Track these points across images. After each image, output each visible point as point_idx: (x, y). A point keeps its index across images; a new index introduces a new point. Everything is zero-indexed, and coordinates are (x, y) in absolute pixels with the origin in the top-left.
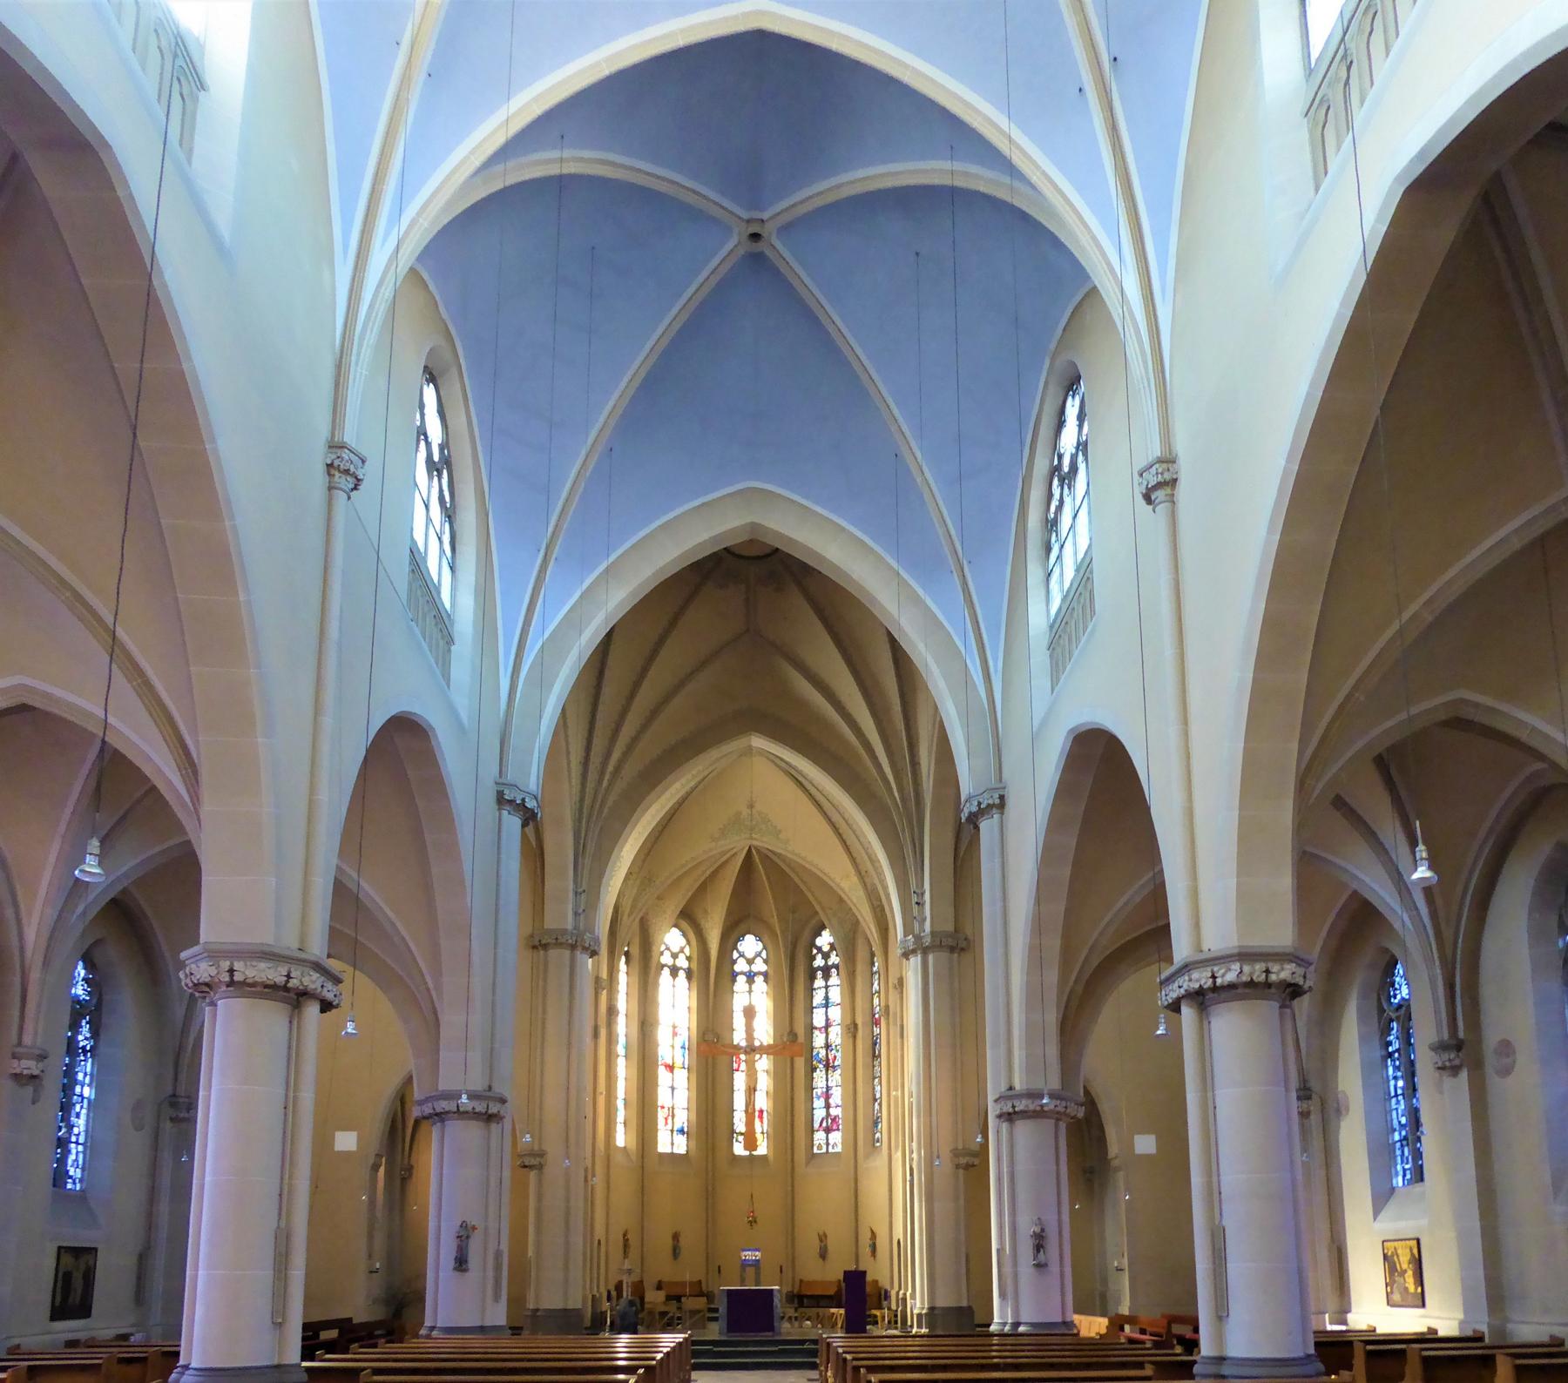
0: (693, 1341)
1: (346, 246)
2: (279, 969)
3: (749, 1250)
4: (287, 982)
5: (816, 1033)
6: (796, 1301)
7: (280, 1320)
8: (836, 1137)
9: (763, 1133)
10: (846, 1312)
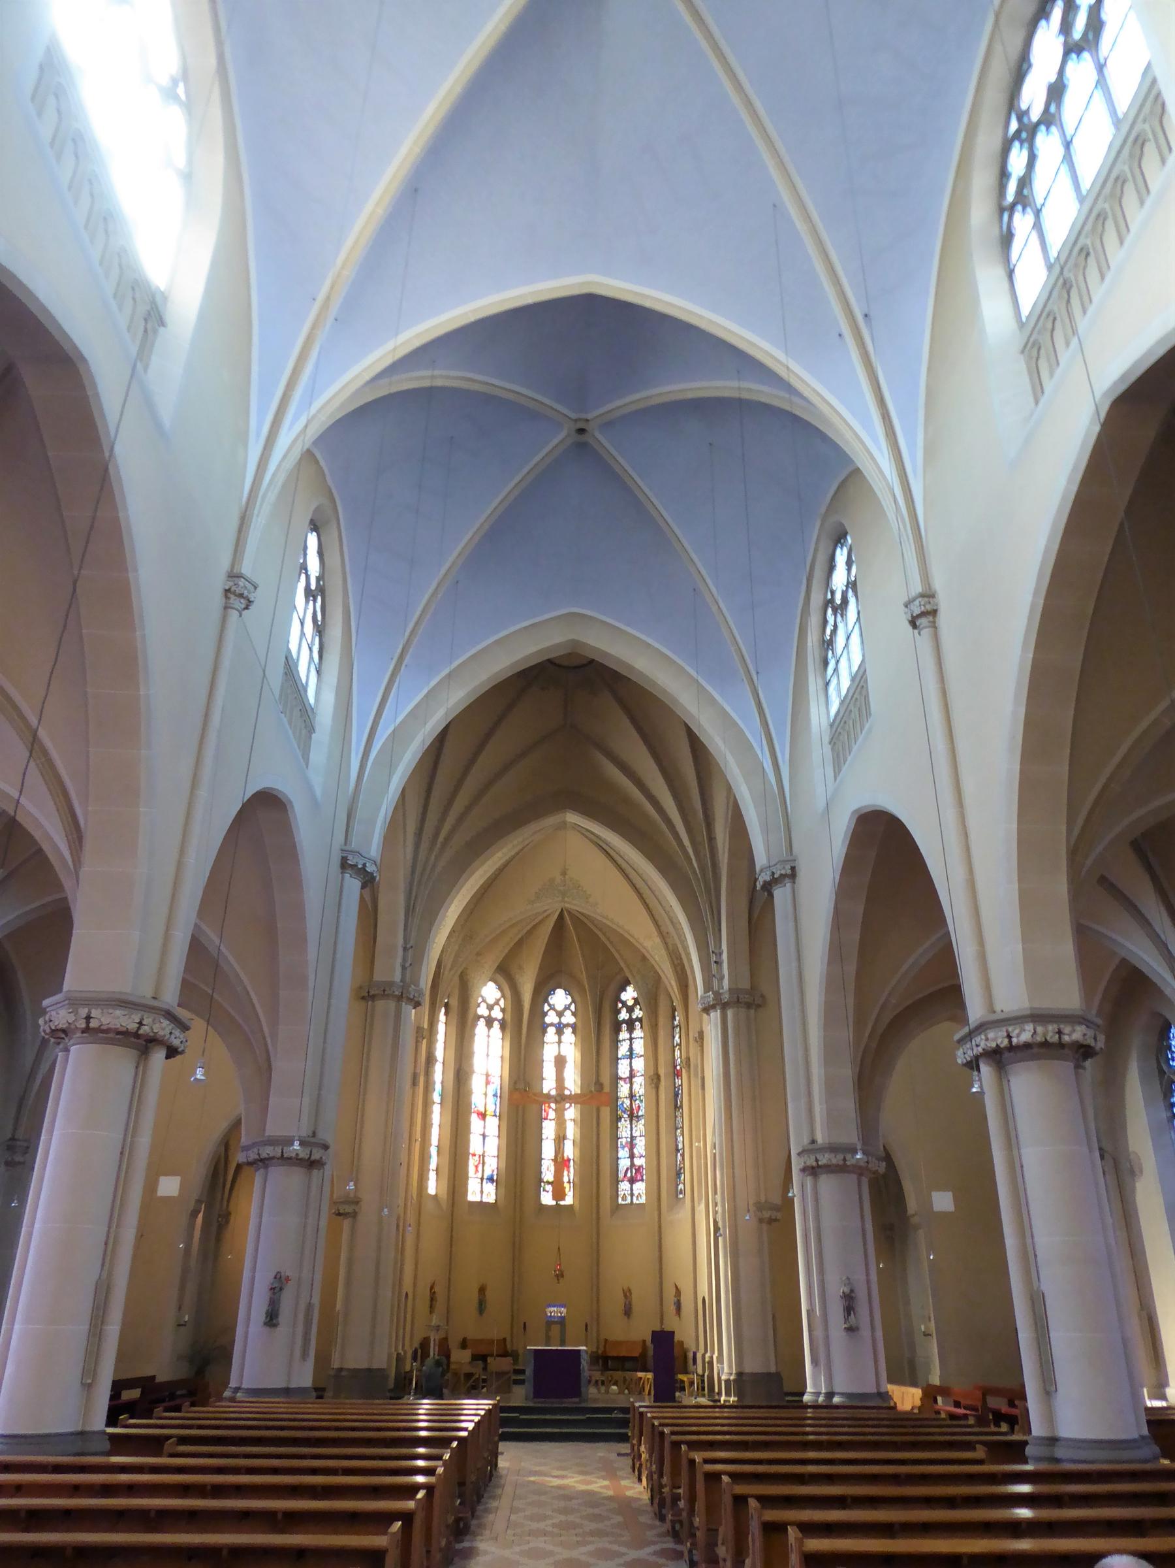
0: (501, 1407)
1: (258, 434)
2: (132, 1016)
3: (554, 1306)
4: (139, 1028)
5: (621, 1083)
6: (600, 1361)
7: (89, 1381)
8: (640, 1187)
9: (569, 1182)
10: (655, 1379)
